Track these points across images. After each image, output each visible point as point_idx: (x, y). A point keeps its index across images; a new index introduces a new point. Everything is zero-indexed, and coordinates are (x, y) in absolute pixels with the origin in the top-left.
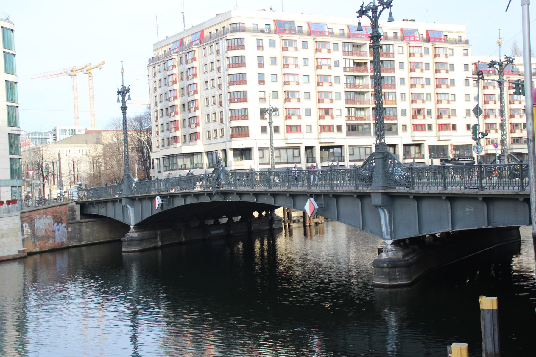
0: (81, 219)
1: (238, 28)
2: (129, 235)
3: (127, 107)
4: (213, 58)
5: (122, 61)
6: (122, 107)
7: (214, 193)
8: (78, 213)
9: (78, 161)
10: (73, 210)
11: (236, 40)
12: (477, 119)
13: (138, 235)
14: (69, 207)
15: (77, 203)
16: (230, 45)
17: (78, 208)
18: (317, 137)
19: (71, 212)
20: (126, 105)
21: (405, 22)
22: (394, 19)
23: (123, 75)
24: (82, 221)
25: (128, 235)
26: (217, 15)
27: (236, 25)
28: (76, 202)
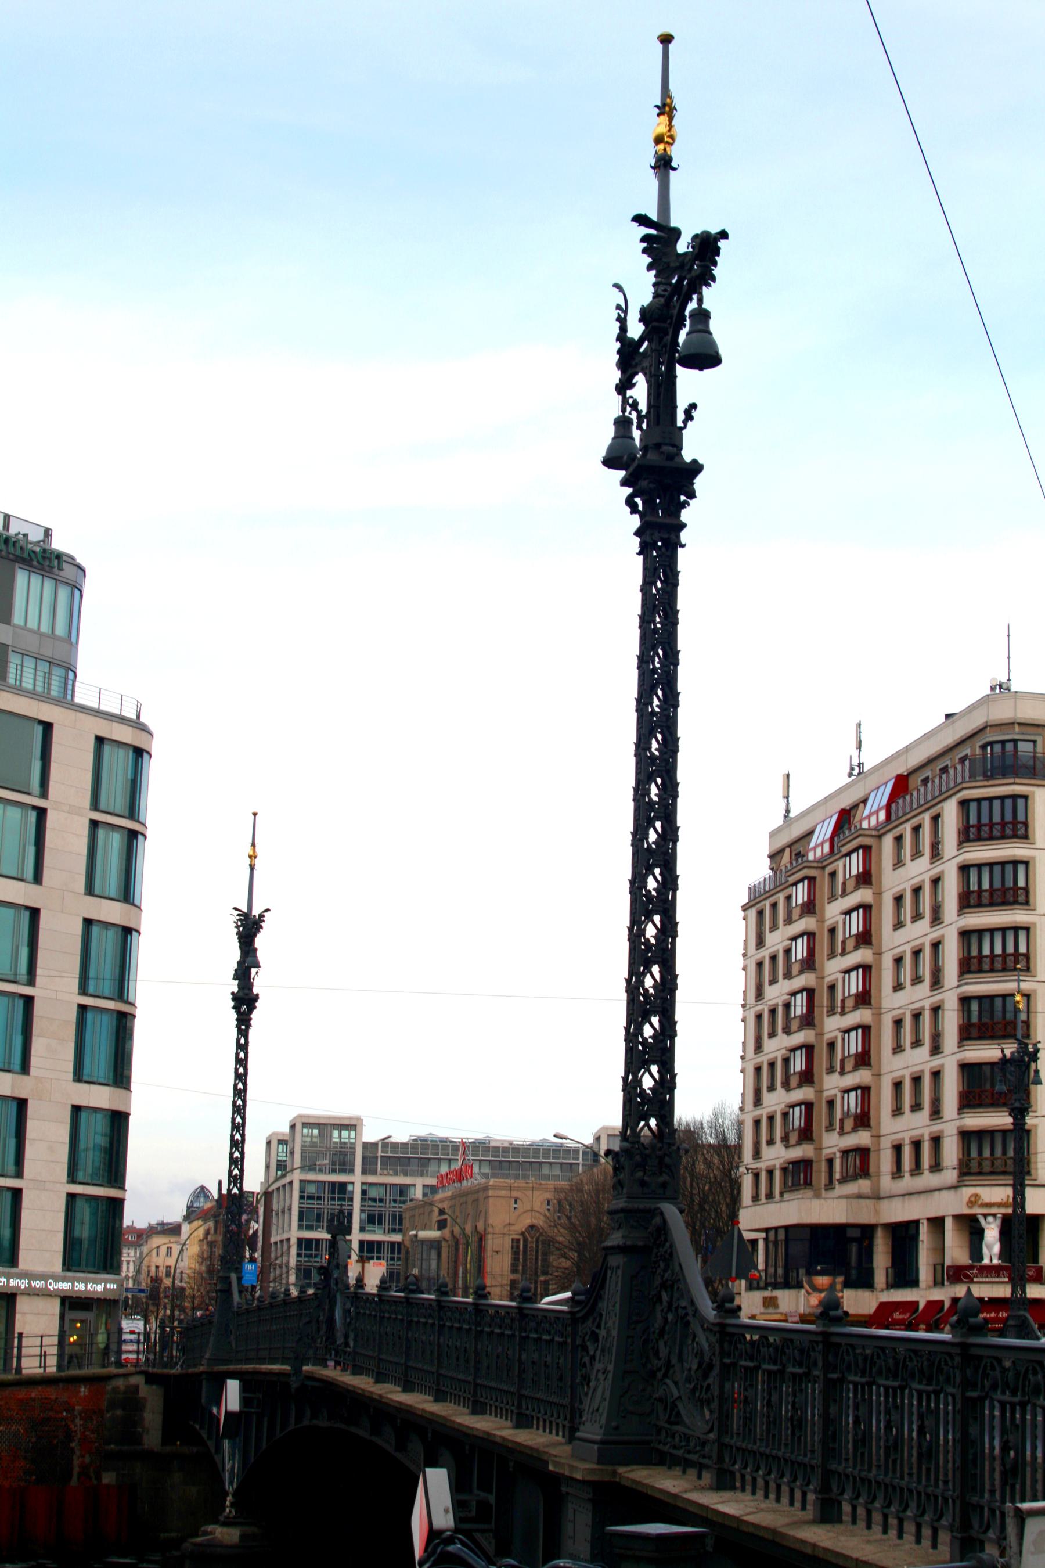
0: (164, 1442)
1: (1009, 762)
2: (211, 1533)
3: (256, 998)
4: (919, 870)
5: (255, 814)
6: (235, 997)
7: (294, 1385)
8: (152, 1418)
9: (541, 1238)
10: (131, 1402)
11: (997, 804)
12: (852, 889)
13: (243, 1537)
14: (115, 1390)
15: (151, 1379)
16: (975, 822)
17: (152, 1397)
18: (882, 1139)
19: (119, 1412)
20: (255, 991)
21: (616, 290)
22: (723, 351)
23: (252, 868)
24: (168, 1449)
25: (206, 1533)
26: (948, 716)
27: (1003, 748)
28: (145, 1373)
